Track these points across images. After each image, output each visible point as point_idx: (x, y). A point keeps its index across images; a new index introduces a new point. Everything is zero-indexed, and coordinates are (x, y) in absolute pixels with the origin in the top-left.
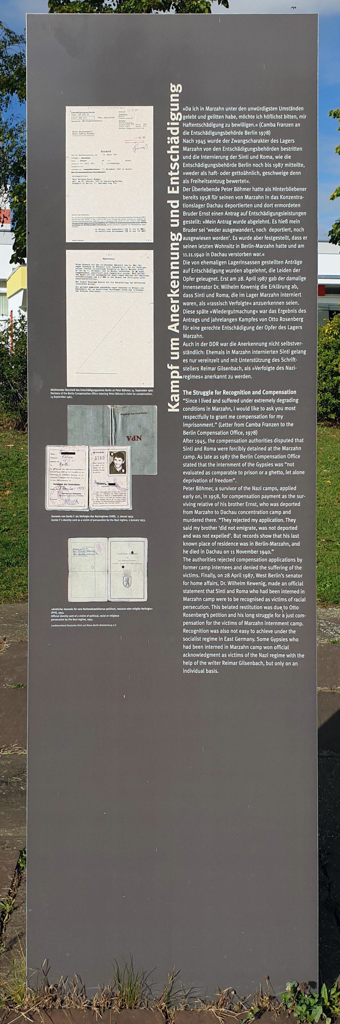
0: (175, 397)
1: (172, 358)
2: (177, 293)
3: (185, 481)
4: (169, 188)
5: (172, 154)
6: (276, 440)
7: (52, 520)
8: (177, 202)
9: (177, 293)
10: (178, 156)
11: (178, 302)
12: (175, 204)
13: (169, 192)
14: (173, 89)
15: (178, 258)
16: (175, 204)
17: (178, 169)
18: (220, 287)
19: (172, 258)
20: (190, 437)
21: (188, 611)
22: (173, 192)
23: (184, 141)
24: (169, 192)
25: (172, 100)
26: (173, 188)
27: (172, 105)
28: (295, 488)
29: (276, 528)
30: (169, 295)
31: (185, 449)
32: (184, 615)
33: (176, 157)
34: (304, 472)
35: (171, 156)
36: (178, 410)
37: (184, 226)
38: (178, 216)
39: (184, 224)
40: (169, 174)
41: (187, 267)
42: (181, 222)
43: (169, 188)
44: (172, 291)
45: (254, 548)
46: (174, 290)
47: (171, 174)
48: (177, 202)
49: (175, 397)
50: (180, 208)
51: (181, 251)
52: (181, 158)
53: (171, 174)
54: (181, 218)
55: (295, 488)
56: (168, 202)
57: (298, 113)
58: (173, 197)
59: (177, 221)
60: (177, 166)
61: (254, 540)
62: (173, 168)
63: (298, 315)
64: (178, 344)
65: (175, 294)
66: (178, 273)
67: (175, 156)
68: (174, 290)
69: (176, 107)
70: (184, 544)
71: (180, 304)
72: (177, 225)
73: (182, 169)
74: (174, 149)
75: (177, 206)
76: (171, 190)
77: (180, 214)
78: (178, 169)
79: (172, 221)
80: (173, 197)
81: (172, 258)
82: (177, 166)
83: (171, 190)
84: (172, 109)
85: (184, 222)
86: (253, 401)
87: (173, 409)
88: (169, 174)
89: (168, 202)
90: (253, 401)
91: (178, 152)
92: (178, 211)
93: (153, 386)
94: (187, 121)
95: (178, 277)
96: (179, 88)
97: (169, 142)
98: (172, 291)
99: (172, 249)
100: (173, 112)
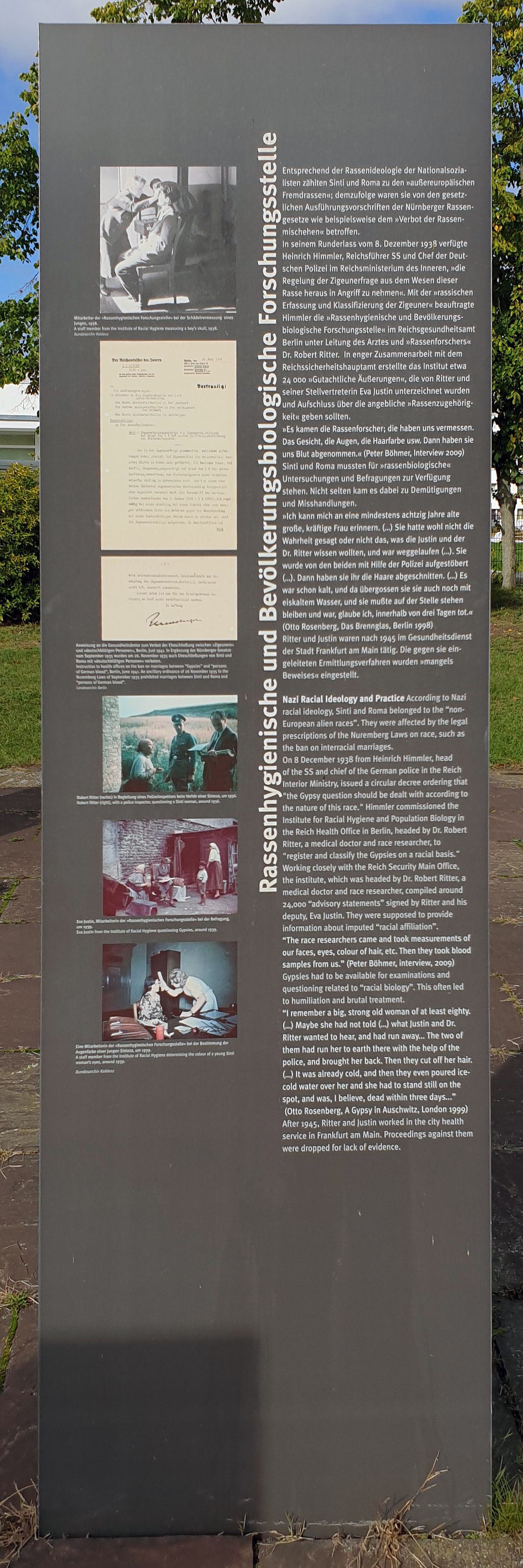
0: (271, 871)
1: (266, 668)
2: (273, 552)
3: (286, 917)
4: (260, 315)
5: (266, 360)
6: (421, 1135)
7: (78, 803)
8: (274, 633)
9: (273, 552)
10: (274, 363)
11: (274, 527)
12: (270, 636)
13: (261, 321)
14: (267, 216)
15: (274, 248)
16: (270, 636)
17: (274, 476)
18: (335, 712)
19: (265, 248)
20: (293, 1118)
21: (290, 912)
22: (268, 618)
23: (285, 342)
24: (261, 321)
25: (266, 234)
26: (267, 316)
27: (265, 511)
28: (450, 758)
29: (422, 220)
30: (260, 426)
31: (286, 1050)
32: (285, 1037)
33: (273, 711)
34: (472, 526)
35: (265, 269)
36: (275, 890)
37: (284, 670)
38: (275, 654)
39: (284, 666)
40: (261, 180)
41: (288, 448)
42: (280, 664)
43: (260, 315)
44: (265, 548)
45: (389, 801)
46: (269, 546)
47: (264, 180)
48: (274, 633)
49: (271, 871)
50: (279, 642)
51: (280, 827)
52: (279, 366)
53: (264, 180)
54: (280, 658)
55: (450, 758)
56: (260, 633)
57: (463, 434)
58: (268, 625)
59: (274, 661)
60: (273, 472)
61: (388, 790)
62: (268, 475)
63: (457, 1066)
64: (275, 809)
65: (269, 552)
66: (275, 740)
67: (270, 363)
68: (269, 546)
69: (272, 515)
70: (284, 417)
71: (279, 531)
72: (274, 668)
73: (281, 730)
74: (269, 806)
75: (275, 639)
76: (264, 318)
77: (279, 651)
78: (275, 862)
79: (266, 661)
80: (268, 625)
81: (265, 248)
82: (273, 379)
83: (264, 318)
84: (265, 518)
85: (284, 663)
86: (388, 976)
87: (267, 887)
88: (261, 180)
89: (260, 633)
90: (388, 976)
91: (274, 357)
92: (274, 349)
93: (236, 639)
94: (289, 226)
95: (275, 747)
96: (277, 779)
97: (261, 577)
98: (265, 548)
99: (266, 504)
100: (268, 771)
